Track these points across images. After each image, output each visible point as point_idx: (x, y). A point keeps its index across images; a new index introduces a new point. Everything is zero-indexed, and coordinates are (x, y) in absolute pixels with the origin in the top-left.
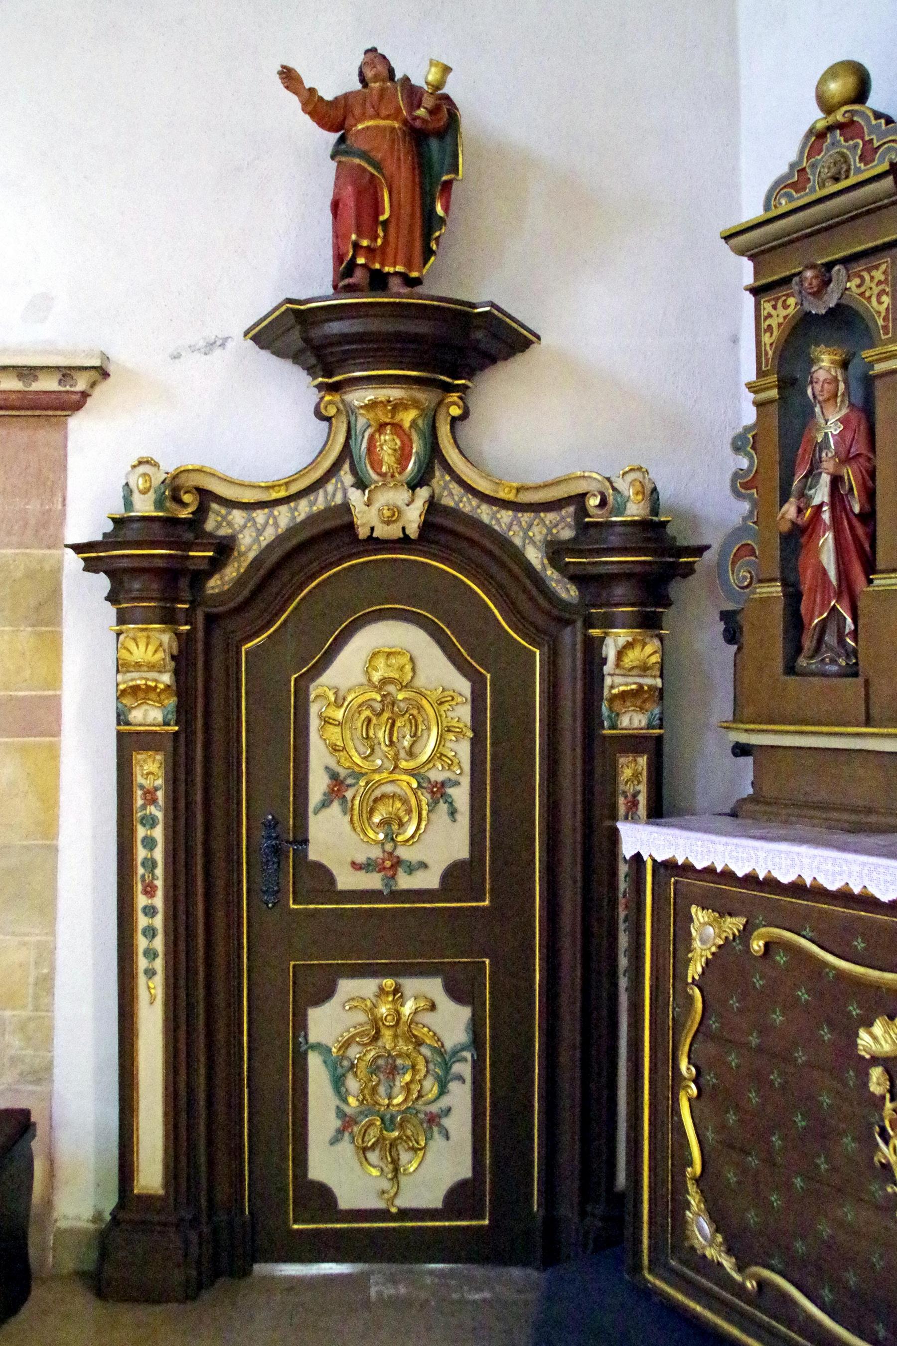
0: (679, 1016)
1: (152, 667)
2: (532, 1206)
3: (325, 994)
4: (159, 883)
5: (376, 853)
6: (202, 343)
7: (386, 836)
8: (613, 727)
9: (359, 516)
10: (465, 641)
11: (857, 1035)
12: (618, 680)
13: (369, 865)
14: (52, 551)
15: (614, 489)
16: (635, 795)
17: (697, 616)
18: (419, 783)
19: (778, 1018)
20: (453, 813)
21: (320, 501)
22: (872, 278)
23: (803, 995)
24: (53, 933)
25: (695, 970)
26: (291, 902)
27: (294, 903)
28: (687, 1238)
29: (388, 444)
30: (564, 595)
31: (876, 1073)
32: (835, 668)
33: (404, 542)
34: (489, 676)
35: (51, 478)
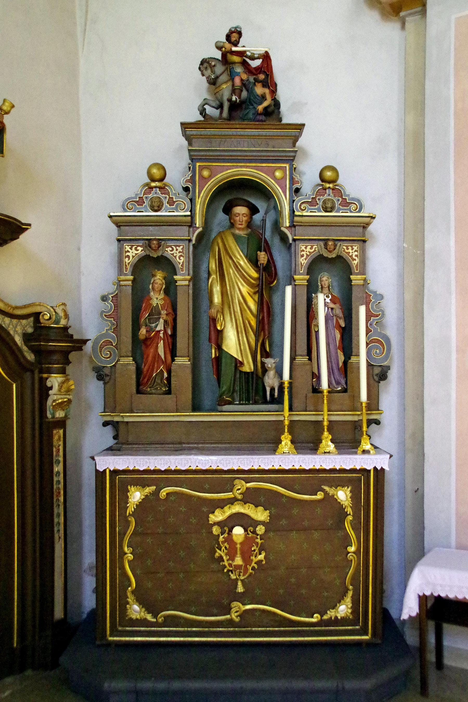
2: (13, 644)
8: (53, 417)
22: (177, 250)
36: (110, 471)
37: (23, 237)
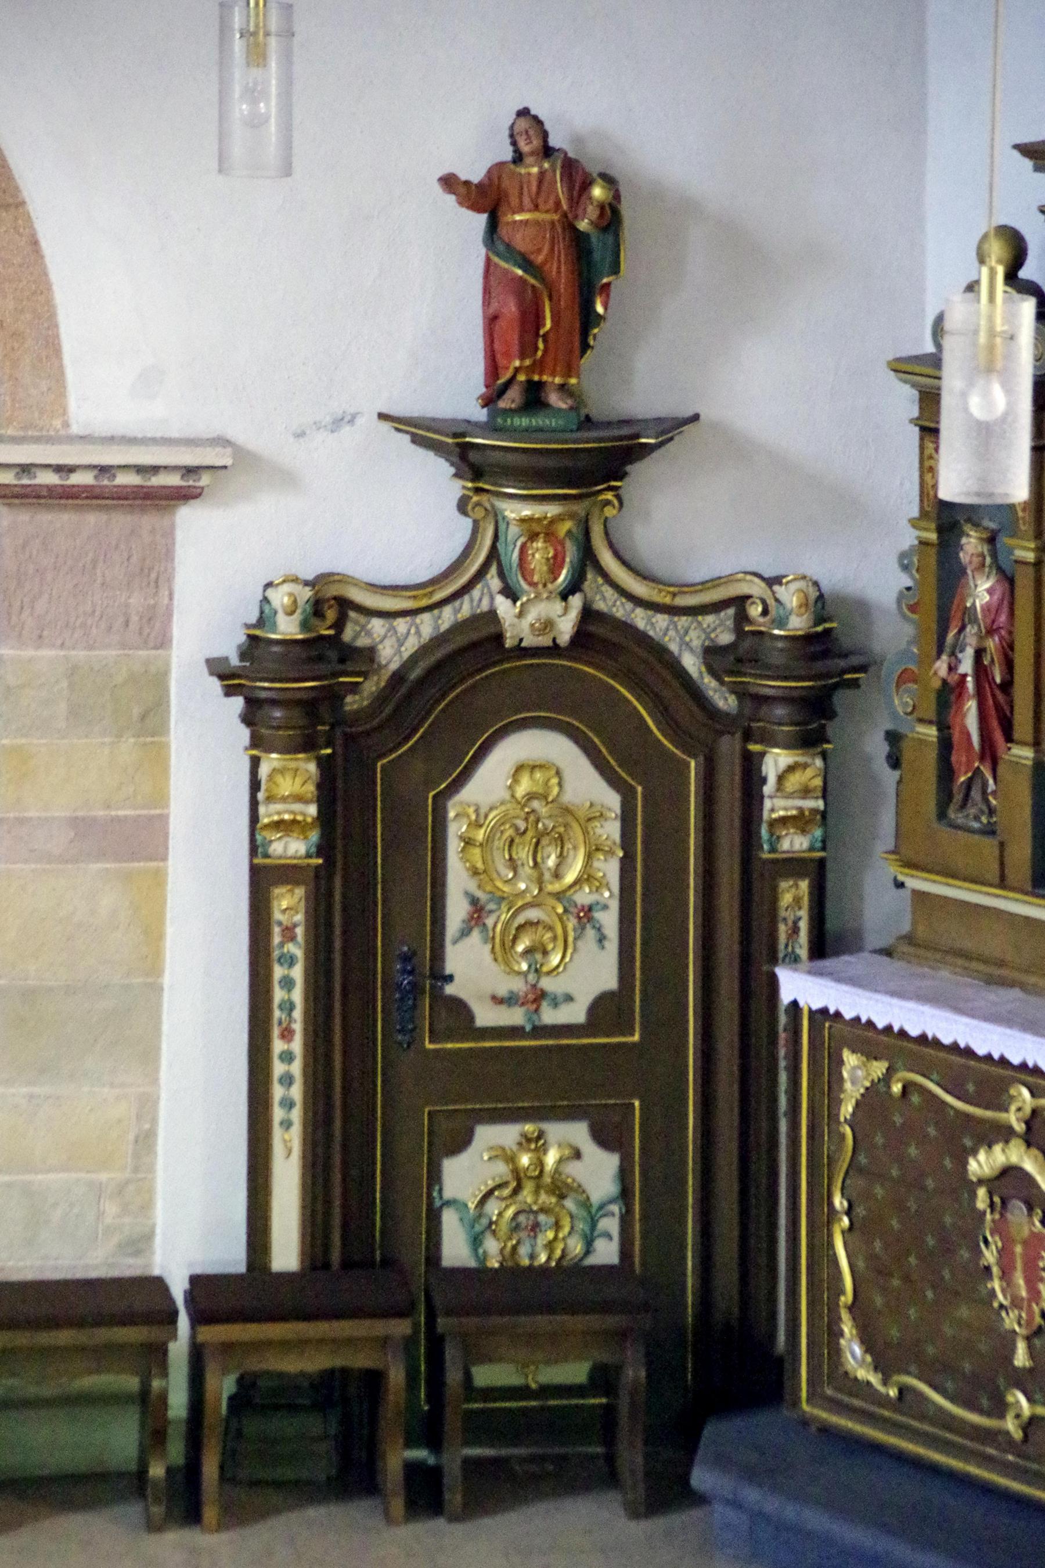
0: (835, 1152)
1: (299, 798)
3: (460, 1142)
4: (298, 1027)
5: (518, 986)
6: (328, 419)
7: (530, 966)
8: (773, 850)
9: (508, 629)
10: (617, 754)
11: (967, 1163)
12: (780, 802)
13: (510, 998)
14: (160, 652)
15: (777, 600)
16: (795, 923)
17: (866, 731)
18: (565, 908)
19: (913, 1151)
20: (601, 939)
21: (465, 608)
23: (932, 1131)
24: (155, 1081)
25: (847, 1109)
26: (427, 1039)
27: (430, 1042)
28: (842, 1365)
29: (539, 554)
30: (721, 704)
31: (982, 1192)
32: (976, 825)
33: (555, 650)
34: (639, 789)
35: (155, 570)
36: (810, 1011)
37: (216, 654)
